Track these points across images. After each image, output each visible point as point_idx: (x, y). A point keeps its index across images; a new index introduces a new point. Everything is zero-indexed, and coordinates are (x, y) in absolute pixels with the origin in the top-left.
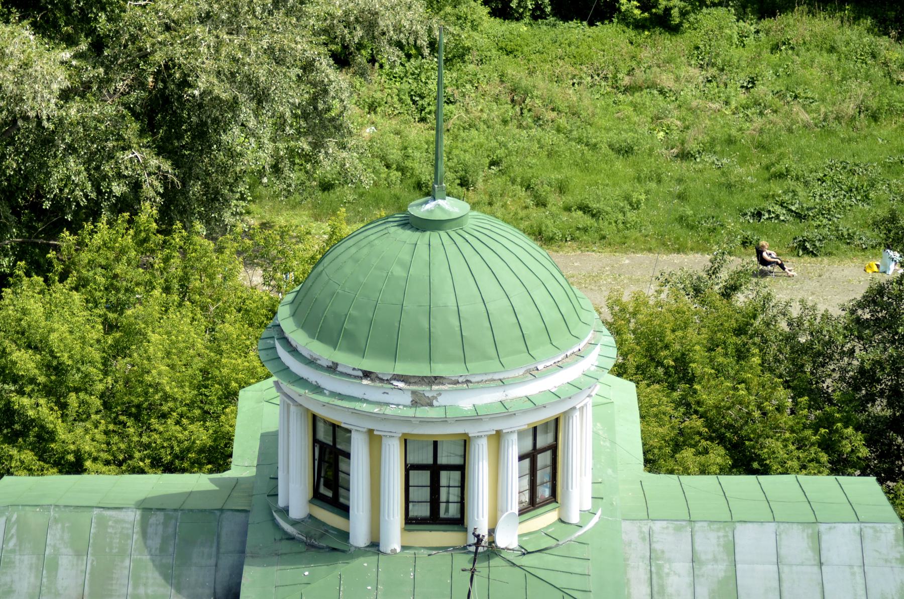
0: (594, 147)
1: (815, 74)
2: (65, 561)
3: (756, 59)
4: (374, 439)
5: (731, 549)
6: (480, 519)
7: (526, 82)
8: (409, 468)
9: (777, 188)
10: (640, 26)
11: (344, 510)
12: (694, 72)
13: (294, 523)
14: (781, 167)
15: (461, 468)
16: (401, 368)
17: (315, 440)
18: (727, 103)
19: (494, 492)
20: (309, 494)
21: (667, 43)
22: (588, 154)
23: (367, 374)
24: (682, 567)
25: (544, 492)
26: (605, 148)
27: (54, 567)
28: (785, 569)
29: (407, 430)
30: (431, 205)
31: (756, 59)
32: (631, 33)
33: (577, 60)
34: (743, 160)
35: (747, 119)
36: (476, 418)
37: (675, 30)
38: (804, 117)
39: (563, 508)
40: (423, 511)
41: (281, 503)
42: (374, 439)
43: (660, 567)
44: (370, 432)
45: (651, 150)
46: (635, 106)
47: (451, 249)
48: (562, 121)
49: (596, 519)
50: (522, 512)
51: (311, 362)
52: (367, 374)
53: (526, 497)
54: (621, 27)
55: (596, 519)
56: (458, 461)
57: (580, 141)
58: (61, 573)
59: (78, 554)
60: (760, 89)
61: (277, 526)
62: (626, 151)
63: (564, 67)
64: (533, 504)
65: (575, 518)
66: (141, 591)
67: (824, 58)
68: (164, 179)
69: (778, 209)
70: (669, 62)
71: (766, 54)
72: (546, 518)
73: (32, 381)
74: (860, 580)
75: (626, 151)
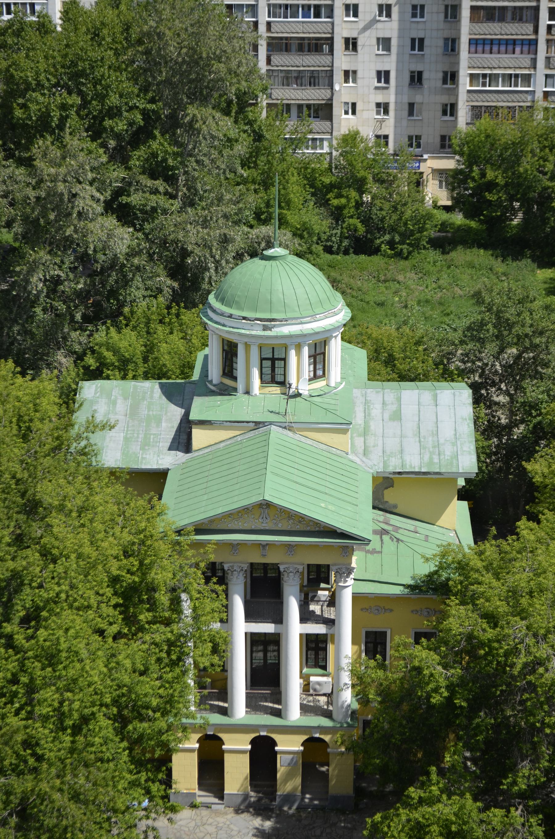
0: (368, 303)
1: (465, 277)
2: (120, 401)
3: (439, 271)
4: (247, 346)
5: (399, 399)
6: (292, 378)
7: (339, 278)
8: (262, 359)
9: (446, 319)
10: (390, 257)
11: (235, 379)
12: (413, 275)
13: (214, 385)
14: (448, 311)
15: (284, 360)
16: (258, 315)
17: (223, 350)
18: (427, 287)
19: (298, 367)
20: (221, 373)
21: (402, 263)
22: (365, 305)
23: (244, 318)
24: (379, 406)
25: (320, 373)
26: (372, 303)
27: (115, 403)
28: (422, 407)
29: (260, 342)
30: (273, 250)
31: (439, 271)
32: (386, 260)
33: (362, 269)
34: (432, 309)
35: (435, 293)
36: (290, 337)
37: (406, 258)
38: (461, 293)
39: (328, 379)
40: (268, 378)
41: (210, 379)
42: (247, 346)
43: (369, 406)
44: (246, 343)
45: (392, 305)
46: (386, 288)
47: (281, 268)
48: (354, 293)
49: (342, 386)
50: (310, 380)
51: (222, 314)
52: (244, 318)
53: (312, 374)
54: (382, 257)
55: (342, 386)
56: (283, 356)
57: (362, 300)
58: (118, 406)
59: (125, 399)
60: (441, 282)
61: (208, 388)
62: (381, 304)
63: (356, 272)
64: (315, 377)
65: (333, 384)
66: (151, 413)
67: (469, 271)
68: (173, 289)
69: (446, 327)
70: (402, 270)
71: (445, 269)
72: (320, 384)
73: (113, 364)
74: (452, 411)
75: (381, 304)
